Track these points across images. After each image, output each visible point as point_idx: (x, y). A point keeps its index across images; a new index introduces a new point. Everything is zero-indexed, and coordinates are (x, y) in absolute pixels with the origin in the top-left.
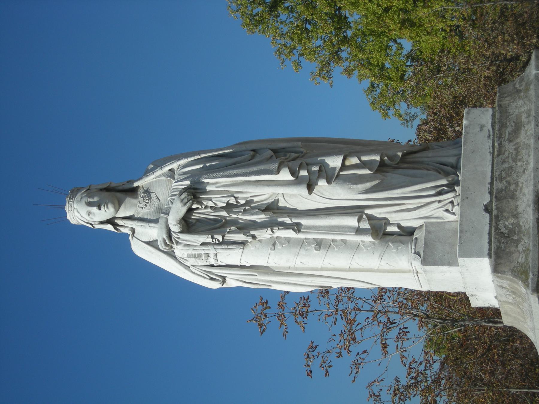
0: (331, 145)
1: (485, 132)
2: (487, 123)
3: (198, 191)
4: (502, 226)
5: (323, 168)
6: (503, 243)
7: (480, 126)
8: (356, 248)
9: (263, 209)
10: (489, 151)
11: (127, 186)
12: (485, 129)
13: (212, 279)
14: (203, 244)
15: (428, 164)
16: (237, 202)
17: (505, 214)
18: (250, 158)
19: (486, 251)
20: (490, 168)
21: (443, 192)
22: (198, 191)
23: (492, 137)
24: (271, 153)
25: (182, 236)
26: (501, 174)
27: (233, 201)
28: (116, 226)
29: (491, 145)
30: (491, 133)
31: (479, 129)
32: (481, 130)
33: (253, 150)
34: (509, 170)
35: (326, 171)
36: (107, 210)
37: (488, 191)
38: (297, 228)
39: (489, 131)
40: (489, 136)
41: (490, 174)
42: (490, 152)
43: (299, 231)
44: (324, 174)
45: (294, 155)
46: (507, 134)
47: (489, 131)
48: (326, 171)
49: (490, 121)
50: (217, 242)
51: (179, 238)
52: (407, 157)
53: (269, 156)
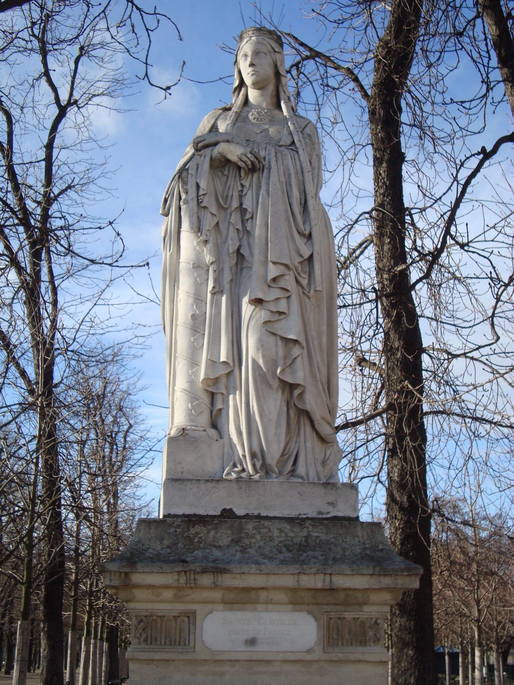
0: (325, 328)
1: (325, 508)
2: (338, 511)
3: (261, 174)
4: (197, 530)
5: (283, 316)
6: (176, 531)
7: (334, 502)
8: (193, 363)
9: (242, 251)
10: (302, 513)
11: (282, 95)
12: (330, 508)
13: (166, 200)
14: (198, 186)
15: (296, 442)
16: (248, 220)
17: (212, 532)
18: (301, 231)
19: (173, 511)
20: (278, 516)
21: (255, 460)
22: (261, 174)
23: (320, 516)
24: (306, 254)
25: (208, 159)
26: (265, 528)
27: (248, 216)
28: (238, 90)
29: (310, 516)
30: (325, 516)
31: (330, 501)
32: (328, 503)
33: (310, 235)
34: (270, 537)
35: (279, 320)
36: (250, 75)
37: (250, 512)
38: (217, 292)
39: (329, 513)
40: (320, 513)
41: (271, 515)
42: (300, 514)
43: (213, 294)
44: (276, 317)
45: (304, 282)
46: (317, 534)
47: (329, 513)
48: (279, 320)
49: (340, 514)
50: (200, 201)
51: (205, 156)
52: (305, 417)
53: (302, 252)
